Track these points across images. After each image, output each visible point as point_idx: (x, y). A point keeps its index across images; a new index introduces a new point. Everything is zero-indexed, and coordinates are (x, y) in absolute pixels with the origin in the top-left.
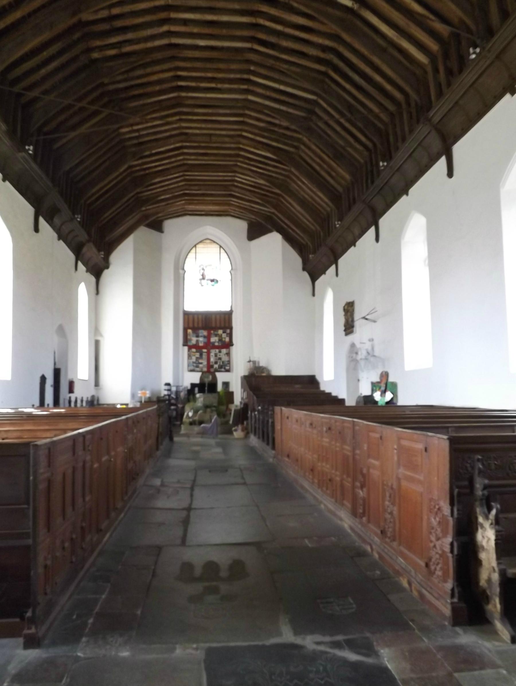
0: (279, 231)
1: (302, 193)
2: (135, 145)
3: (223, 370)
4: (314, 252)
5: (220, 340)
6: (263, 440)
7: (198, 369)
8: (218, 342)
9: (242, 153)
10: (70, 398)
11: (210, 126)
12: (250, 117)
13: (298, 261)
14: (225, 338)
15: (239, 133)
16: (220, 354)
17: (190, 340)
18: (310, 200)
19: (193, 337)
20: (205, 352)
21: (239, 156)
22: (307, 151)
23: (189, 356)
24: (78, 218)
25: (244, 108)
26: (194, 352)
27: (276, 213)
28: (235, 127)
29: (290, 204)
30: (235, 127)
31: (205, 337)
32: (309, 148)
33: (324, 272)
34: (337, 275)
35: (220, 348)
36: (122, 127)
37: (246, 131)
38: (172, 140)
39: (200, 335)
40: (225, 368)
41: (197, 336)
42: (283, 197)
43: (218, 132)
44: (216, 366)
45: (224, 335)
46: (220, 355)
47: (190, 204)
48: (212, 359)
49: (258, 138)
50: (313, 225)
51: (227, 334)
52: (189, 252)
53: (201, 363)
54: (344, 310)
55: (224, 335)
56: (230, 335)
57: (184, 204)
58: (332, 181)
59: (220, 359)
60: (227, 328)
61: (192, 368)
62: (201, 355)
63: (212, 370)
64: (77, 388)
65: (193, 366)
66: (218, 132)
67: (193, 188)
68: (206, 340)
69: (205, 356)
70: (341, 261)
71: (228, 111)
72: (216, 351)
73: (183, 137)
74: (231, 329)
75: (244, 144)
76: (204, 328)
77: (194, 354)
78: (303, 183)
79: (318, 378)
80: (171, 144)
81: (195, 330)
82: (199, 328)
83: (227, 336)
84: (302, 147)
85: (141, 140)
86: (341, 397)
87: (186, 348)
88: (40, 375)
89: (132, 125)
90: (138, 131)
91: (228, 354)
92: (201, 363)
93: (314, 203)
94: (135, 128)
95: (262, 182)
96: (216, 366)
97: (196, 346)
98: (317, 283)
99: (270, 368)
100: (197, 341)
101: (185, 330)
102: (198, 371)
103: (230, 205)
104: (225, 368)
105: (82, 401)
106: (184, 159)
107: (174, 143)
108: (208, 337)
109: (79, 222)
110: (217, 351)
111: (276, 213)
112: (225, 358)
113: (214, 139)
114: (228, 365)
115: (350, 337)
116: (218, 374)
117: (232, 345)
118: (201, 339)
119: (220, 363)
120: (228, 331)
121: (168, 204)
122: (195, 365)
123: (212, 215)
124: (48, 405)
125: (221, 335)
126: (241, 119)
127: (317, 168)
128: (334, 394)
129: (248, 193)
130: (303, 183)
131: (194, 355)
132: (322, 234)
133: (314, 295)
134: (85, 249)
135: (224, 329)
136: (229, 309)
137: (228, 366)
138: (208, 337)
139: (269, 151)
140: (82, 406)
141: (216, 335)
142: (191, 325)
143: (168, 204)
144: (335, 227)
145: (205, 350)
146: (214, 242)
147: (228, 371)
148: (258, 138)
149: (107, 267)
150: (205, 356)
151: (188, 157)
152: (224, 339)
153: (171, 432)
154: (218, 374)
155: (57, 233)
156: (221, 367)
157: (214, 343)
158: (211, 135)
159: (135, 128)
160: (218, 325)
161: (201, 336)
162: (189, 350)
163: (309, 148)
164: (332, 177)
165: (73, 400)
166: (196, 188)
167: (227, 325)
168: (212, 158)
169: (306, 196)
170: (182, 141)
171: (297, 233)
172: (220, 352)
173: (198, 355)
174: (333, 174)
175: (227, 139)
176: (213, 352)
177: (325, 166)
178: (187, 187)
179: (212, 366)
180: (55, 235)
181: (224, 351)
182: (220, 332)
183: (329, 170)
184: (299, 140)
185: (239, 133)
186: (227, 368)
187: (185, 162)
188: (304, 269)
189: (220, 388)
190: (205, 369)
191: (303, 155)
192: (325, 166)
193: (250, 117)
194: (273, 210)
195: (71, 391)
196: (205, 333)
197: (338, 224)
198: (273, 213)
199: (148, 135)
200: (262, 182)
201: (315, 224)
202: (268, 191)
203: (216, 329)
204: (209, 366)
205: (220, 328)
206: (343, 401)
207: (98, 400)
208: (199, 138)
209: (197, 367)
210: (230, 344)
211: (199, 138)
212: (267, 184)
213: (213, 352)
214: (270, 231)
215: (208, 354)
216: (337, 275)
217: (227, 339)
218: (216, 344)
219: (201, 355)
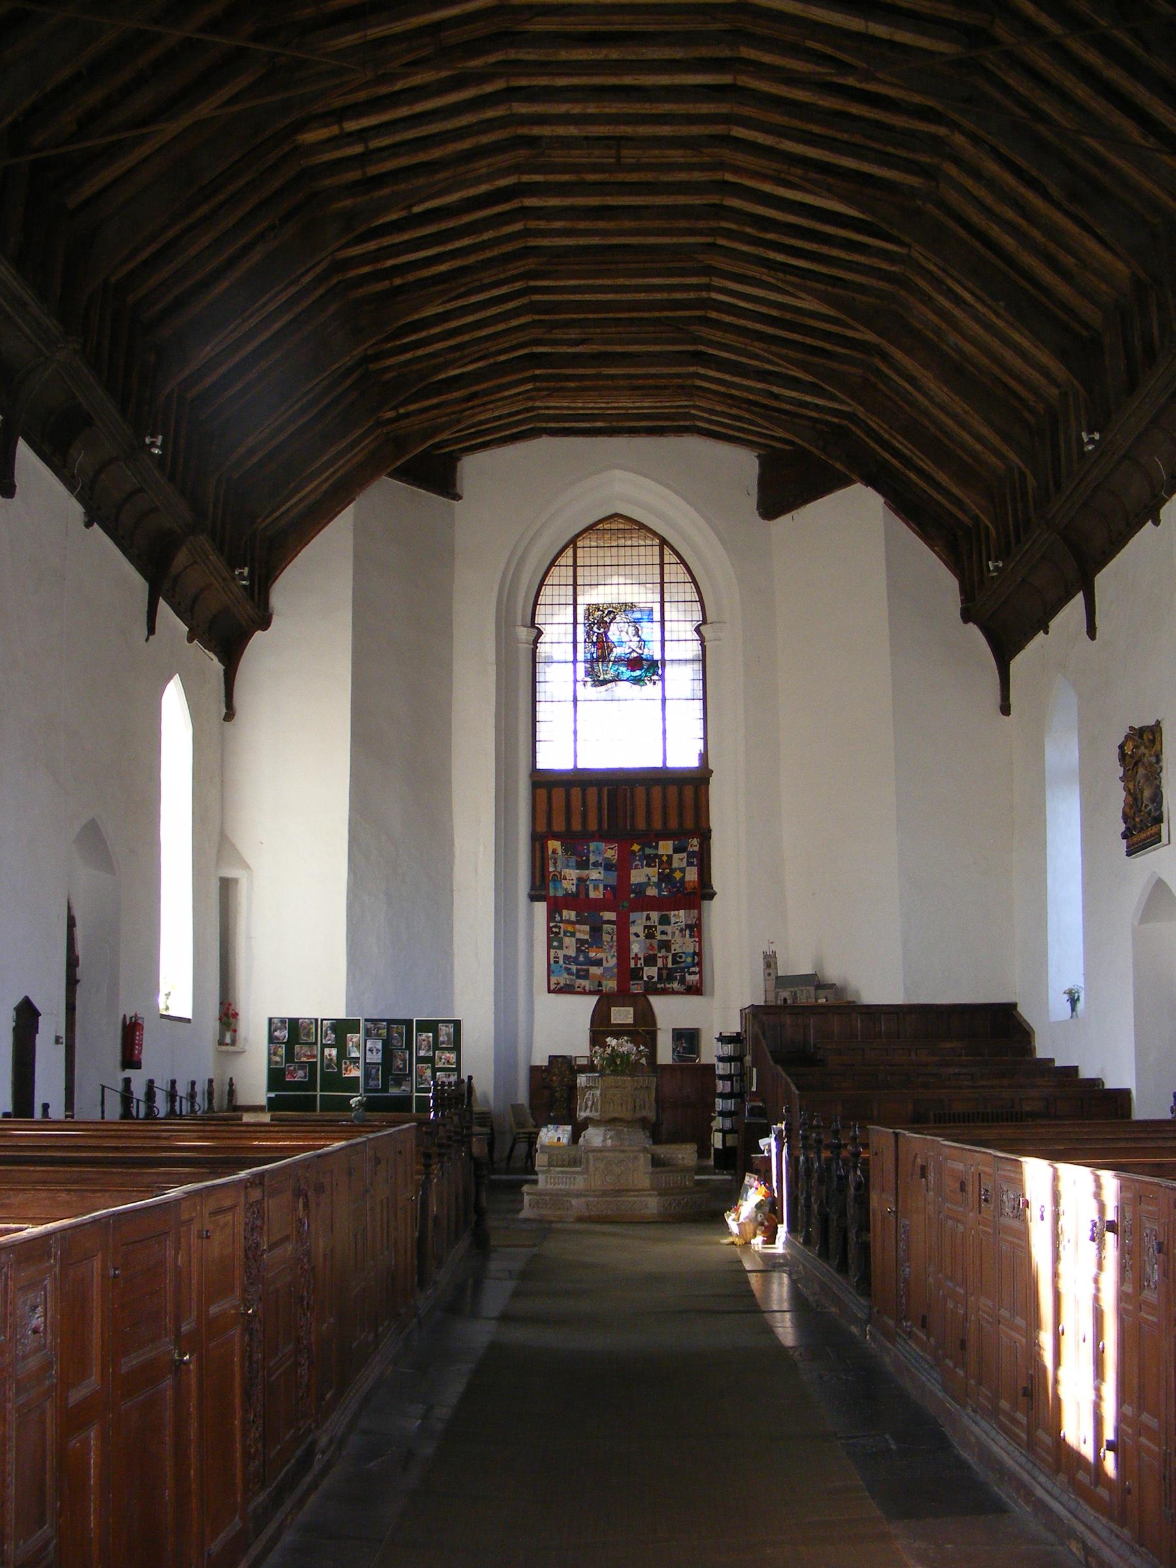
0: (871, 481)
1: (953, 338)
2: (353, 188)
3: (675, 985)
4: (1004, 553)
5: (665, 878)
6: (824, 1254)
7: (586, 983)
8: (658, 885)
9: (736, 203)
10: (127, 1081)
11: (613, 108)
12: (759, 69)
13: (948, 584)
14: (683, 870)
15: (720, 129)
16: (665, 928)
17: (558, 878)
18: (984, 361)
19: (568, 866)
20: (609, 922)
21: (718, 211)
22: (969, 183)
23: (553, 937)
24: (153, 445)
25: (738, 35)
26: (569, 922)
27: (860, 411)
28: (705, 108)
29: (912, 380)
30: (705, 108)
31: (608, 866)
32: (976, 174)
33: (1043, 626)
34: (1092, 631)
35: (662, 905)
36: (302, 125)
37: (745, 122)
38: (482, 166)
39: (592, 859)
40: (682, 981)
41: (583, 865)
42: (885, 357)
43: (643, 130)
44: (651, 972)
45: (679, 860)
46: (663, 933)
47: (552, 393)
48: (636, 948)
49: (788, 146)
50: (995, 451)
51: (691, 855)
52: (552, 564)
53: (598, 963)
54: (1123, 756)
55: (679, 860)
56: (703, 860)
57: (529, 396)
58: (1063, 290)
59: (666, 945)
60: (693, 835)
61: (563, 979)
62: (596, 931)
63: (636, 988)
64: (149, 1051)
65: (568, 970)
66: (643, 130)
67: (558, 334)
68: (612, 878)
69: (609, 934)
70: (1103, 580)
71: (679, 54)
72: (648, 918)
73: (522, 154)
74: (705, 836)
75: (737, 170)
76: (603, 836)
77: (570, 929)
78: (958, 300)
79: (1024, 1011)
80: (479, 180)
81: (575, 842)
82: (587, 836)
83: (690, 864)
84: (952, 170)
85: (373, 170)
86: (1112, 1083)
87: (541, 908)
88: (17, 1000)
89: (340, 115)
90: (362, 135)
91: (696, 929)
92: (598, 963)
93: (997, 371)
94: (351, 126)
95: (809, 303)
96: (651, 972)
97: (578, 901)
98: (1017, 664)
99: (833, 973)
100: (581, 880)
101: (538, 840)
102: (584, 992)
103: (690, 391)
104: (682, 981)
105: (172, 1095)
106: (527, 233)
107: (490, 177)
108: (622, 867)
109: (160, 460)
110: (655, 916)
111: (860, 411)
112: (683, 944)
113: (629, 155)
114: (696, 969)
115: (1152, 861)
116: (656, 1001)
117: (711, 896)
118: (595, 874)
119: (665, 960)
120: (694, 844)
121: (474, 396)
122: (574, 968)
123: (633, 432)
124: (46, 1107)
125: (670, 857)
126: (725, 79)
127: (1009, 242)
128: (1087, 1072)
129: (757, 347)
130: (958, 300)
131: (573, 934)
132: (1031, 481)
133: (1005, 709)
134: (182, 558)
135: (680, 837)
136: (693, 762)
137: (694, 973)
138: (622, 867)
139: (830, 191)
140: (150, 1114)
141: (650, 861)
142: (559, 826)
143: (474, 396)
144: (1083, 454)
145: (610, 916)
146: (642, 526)
147: (695, 990)
148: (788, 146)
149: (264, 622)
150: (609, 934)
151: (542, 224)
152: (678, 875)
153: (480, 1212)
154: (656, 1001)
155: (80, 498)
156: (667, 975)
157: (641, 888)
158: (619, 141)
159: (351, 126)
160: (658, 825)
161: (596, 864)
162: (550, 918)
163: (976, 174)
164: (1066, 275)
165: (138, 1090)
166: (573, 334)
167: (689, 824)
168: (628, 224)
169: (969, 349)
170: (517, 169)
171: (938, 487)
172: (665, 920)
173: (583, 931)
174: (1069, 261)
175: (676, 155)
176: (638, 923)
177: (1036, 233)
178: (537, 333)
179: (636, 974)
180: (77, 509)
181: (680, 917)
182: (665, 847)
183: (1052, 248)
184: (937, 145)
185: (720, 129)
186: (692, 979)
187: (532, 242)
188: (967, 616)
189: (665, 1054)
190: (611, 985)
191: (953, 197)
192: (1036, 233)
193: (759, 69)
194: (850, 406)
195: (130, 1060)
196: (611, 853)
197: (1089, 440)
198: (850, 417)
199: (395, 149)
200: (809, 303)
201: (1004, 449)
202: (827, 336)
203: (650, 838)
204: (627, 972)
205: (666, 836)
206: (1123, 1096)
207: (232, 1092)
208: (576, 156)
209: (585, 975)
210: (704, 891)
211: (576, 156)
212: (832, 312)
213: (638, 923)
214: (844, 482)
215: (623, 927)
216: (1092, 631)
217: (692, 875)
218: (652, 892)
219: (596, 931)
